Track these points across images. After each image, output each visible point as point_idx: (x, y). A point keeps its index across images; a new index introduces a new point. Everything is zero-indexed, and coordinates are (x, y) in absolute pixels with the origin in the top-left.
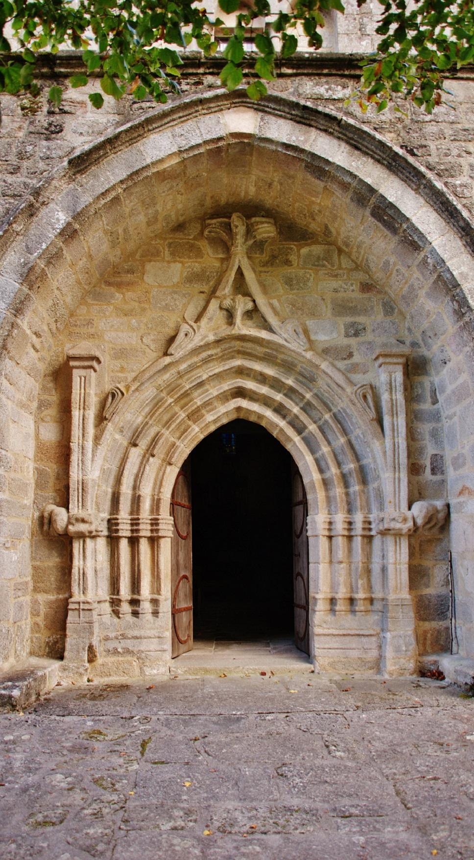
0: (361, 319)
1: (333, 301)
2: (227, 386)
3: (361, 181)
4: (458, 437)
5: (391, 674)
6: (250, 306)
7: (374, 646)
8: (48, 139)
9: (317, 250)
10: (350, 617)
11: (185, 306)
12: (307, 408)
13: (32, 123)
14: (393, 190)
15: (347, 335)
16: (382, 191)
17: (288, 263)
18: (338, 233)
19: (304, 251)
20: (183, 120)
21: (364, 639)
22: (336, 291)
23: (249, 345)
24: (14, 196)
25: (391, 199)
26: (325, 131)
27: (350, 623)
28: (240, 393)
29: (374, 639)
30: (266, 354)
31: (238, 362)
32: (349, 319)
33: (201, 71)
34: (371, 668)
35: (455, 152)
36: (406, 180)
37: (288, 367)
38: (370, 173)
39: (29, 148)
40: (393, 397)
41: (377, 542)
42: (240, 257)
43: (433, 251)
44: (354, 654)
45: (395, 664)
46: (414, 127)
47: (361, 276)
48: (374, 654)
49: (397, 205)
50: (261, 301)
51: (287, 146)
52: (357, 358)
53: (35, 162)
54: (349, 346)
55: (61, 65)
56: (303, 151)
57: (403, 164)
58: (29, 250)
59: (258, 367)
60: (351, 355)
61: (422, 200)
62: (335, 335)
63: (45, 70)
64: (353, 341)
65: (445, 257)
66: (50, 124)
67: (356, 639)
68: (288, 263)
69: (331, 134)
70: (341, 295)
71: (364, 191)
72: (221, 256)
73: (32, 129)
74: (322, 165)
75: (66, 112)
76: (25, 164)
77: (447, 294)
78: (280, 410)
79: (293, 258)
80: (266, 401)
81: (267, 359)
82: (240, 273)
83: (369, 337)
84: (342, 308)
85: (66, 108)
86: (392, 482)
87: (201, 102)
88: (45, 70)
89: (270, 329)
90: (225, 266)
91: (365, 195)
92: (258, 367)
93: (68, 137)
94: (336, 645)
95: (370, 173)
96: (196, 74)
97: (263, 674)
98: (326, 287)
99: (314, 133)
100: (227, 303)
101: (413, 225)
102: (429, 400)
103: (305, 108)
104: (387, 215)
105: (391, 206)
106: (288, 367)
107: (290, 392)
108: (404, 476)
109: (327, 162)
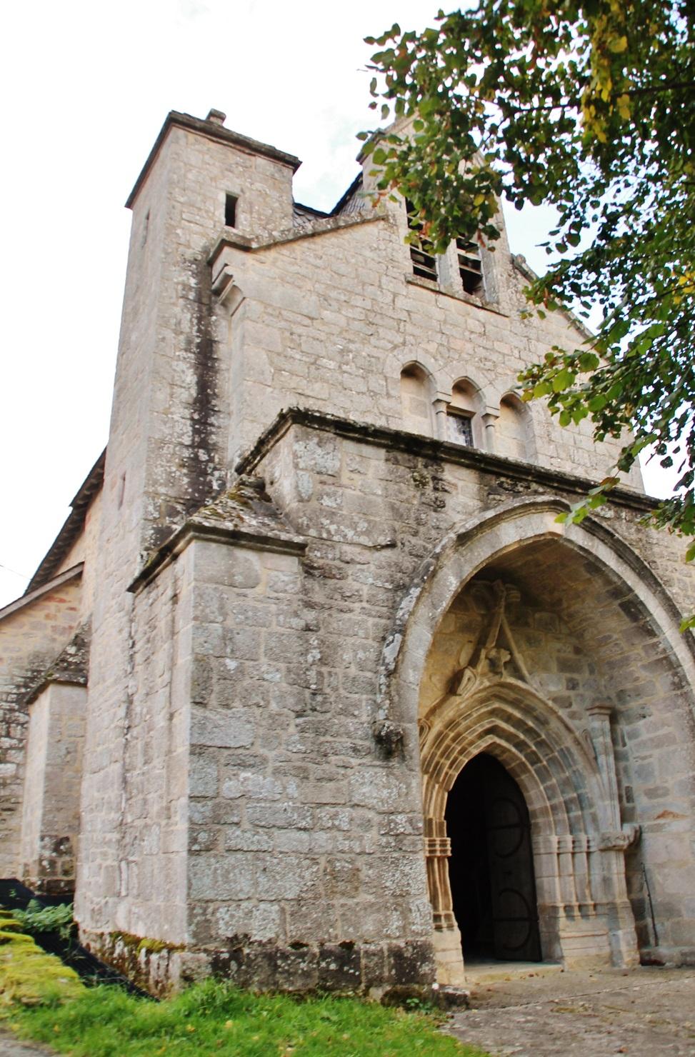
0: (576, 676)
1: (558, 659)
2: (487, 725)
3: (624, 583)
4: (656, 773)
5: (627, 964)
6: (508, 657)
7: (607, 943)
8: (435, 511)
9: (545, 615)
10: (584, 921)
11: (459, 653)
12: (541, 744)
13: (423, 494)
14: (643, 592)
15: (568, 688)
16: (637, 592)
17: (527, 624)
18: (568, 607)
19: (537, 616)
20: (522, 515)
21: (598, 939)
22: (559, 651)
23: (505, 691)
24: (417, 556)
25: (642, 599)
26: (602, 541)
27: (584, 926)
28: (493, 730)
29: (605, 938)
30: (516, 699)
31: (497, 705)
32: (568, 675)
33: (530, 478)
34: (606, 963)
35: (670, 569)
36: (649, 585)
37: (528, 710)
38: (631, 579)
39: (423, 516)
40: (603, 741)
41: (596, 858)
42: (502, 617)
43: (665, 639)
44: (593, 952)
45: (629, 956)
46: (648, 546)
47: (574, 641)
48: (606, 950)
49: (645, 603)
50: (518, 656)
51: (581, 548)
52: (575, 707)
53: (429, 530)
54: (569, 697)
55: (443, 452)
56: (590, 553)
57: (648, 574)
58: (435, 606)
59: (510, 710)
60: (570, 705)
61: (657, 601)
62: (560, 687)
63: (430, 452)
64: (571, 693)
65: (673, 644)
66: (436, 499)
67: (591, 938)
68: (527, 624)
69: (606, 544)
70: (563, 655)
71: (625, 589)
72: (482, 612)
73: (424, 500)
74: (600, 565)
75: (446, 491)
76: (422, 529)
77: (670, 670)
78: (520, 745)
79: (530, 620)
80: (509, 737)
81: (515, 703)
82: (502, 632)
83: (581, 690)
84: (565, 666)
85: (447, 488)
86: (608, 810)
87: (534, 504)
88: (430, 452)
89: (522, 678)
90: (486, 622)
91: (620, 593)
92: (510, 710)
93: (450, 512)
94: (579, 946)
95: (631, 579)
96: (527, 480)
97: (532, 976)
98: (556, 647)
99: (597, 542)
100: (493, 653)
101: (654, 620)
102: (621, 744)
103: (595, 522)
104: (634, 609)
105: (641, 603)
106: (528, 710)
107: (529, 731)
108: (616, 802)
109: (605, 564)
